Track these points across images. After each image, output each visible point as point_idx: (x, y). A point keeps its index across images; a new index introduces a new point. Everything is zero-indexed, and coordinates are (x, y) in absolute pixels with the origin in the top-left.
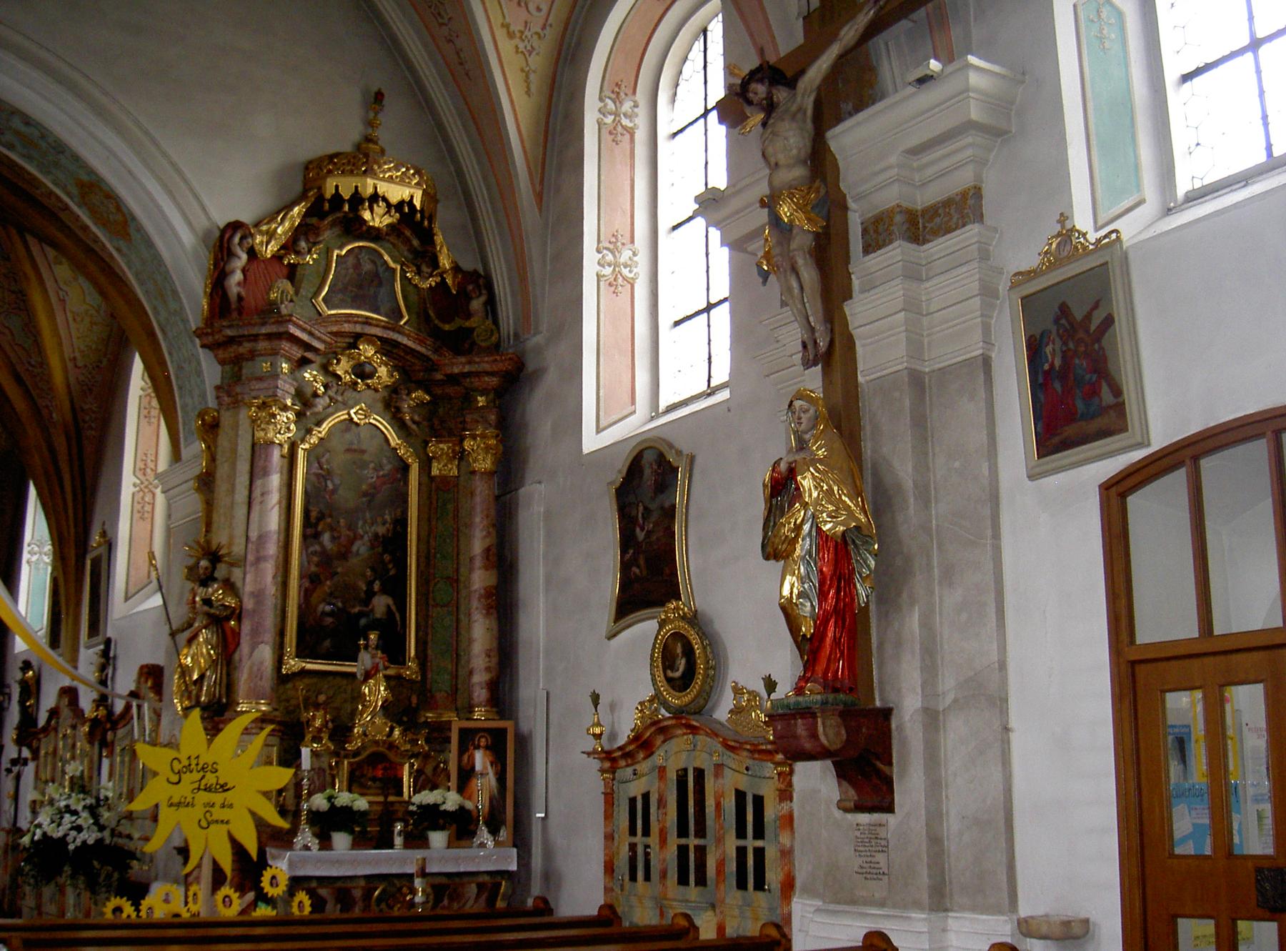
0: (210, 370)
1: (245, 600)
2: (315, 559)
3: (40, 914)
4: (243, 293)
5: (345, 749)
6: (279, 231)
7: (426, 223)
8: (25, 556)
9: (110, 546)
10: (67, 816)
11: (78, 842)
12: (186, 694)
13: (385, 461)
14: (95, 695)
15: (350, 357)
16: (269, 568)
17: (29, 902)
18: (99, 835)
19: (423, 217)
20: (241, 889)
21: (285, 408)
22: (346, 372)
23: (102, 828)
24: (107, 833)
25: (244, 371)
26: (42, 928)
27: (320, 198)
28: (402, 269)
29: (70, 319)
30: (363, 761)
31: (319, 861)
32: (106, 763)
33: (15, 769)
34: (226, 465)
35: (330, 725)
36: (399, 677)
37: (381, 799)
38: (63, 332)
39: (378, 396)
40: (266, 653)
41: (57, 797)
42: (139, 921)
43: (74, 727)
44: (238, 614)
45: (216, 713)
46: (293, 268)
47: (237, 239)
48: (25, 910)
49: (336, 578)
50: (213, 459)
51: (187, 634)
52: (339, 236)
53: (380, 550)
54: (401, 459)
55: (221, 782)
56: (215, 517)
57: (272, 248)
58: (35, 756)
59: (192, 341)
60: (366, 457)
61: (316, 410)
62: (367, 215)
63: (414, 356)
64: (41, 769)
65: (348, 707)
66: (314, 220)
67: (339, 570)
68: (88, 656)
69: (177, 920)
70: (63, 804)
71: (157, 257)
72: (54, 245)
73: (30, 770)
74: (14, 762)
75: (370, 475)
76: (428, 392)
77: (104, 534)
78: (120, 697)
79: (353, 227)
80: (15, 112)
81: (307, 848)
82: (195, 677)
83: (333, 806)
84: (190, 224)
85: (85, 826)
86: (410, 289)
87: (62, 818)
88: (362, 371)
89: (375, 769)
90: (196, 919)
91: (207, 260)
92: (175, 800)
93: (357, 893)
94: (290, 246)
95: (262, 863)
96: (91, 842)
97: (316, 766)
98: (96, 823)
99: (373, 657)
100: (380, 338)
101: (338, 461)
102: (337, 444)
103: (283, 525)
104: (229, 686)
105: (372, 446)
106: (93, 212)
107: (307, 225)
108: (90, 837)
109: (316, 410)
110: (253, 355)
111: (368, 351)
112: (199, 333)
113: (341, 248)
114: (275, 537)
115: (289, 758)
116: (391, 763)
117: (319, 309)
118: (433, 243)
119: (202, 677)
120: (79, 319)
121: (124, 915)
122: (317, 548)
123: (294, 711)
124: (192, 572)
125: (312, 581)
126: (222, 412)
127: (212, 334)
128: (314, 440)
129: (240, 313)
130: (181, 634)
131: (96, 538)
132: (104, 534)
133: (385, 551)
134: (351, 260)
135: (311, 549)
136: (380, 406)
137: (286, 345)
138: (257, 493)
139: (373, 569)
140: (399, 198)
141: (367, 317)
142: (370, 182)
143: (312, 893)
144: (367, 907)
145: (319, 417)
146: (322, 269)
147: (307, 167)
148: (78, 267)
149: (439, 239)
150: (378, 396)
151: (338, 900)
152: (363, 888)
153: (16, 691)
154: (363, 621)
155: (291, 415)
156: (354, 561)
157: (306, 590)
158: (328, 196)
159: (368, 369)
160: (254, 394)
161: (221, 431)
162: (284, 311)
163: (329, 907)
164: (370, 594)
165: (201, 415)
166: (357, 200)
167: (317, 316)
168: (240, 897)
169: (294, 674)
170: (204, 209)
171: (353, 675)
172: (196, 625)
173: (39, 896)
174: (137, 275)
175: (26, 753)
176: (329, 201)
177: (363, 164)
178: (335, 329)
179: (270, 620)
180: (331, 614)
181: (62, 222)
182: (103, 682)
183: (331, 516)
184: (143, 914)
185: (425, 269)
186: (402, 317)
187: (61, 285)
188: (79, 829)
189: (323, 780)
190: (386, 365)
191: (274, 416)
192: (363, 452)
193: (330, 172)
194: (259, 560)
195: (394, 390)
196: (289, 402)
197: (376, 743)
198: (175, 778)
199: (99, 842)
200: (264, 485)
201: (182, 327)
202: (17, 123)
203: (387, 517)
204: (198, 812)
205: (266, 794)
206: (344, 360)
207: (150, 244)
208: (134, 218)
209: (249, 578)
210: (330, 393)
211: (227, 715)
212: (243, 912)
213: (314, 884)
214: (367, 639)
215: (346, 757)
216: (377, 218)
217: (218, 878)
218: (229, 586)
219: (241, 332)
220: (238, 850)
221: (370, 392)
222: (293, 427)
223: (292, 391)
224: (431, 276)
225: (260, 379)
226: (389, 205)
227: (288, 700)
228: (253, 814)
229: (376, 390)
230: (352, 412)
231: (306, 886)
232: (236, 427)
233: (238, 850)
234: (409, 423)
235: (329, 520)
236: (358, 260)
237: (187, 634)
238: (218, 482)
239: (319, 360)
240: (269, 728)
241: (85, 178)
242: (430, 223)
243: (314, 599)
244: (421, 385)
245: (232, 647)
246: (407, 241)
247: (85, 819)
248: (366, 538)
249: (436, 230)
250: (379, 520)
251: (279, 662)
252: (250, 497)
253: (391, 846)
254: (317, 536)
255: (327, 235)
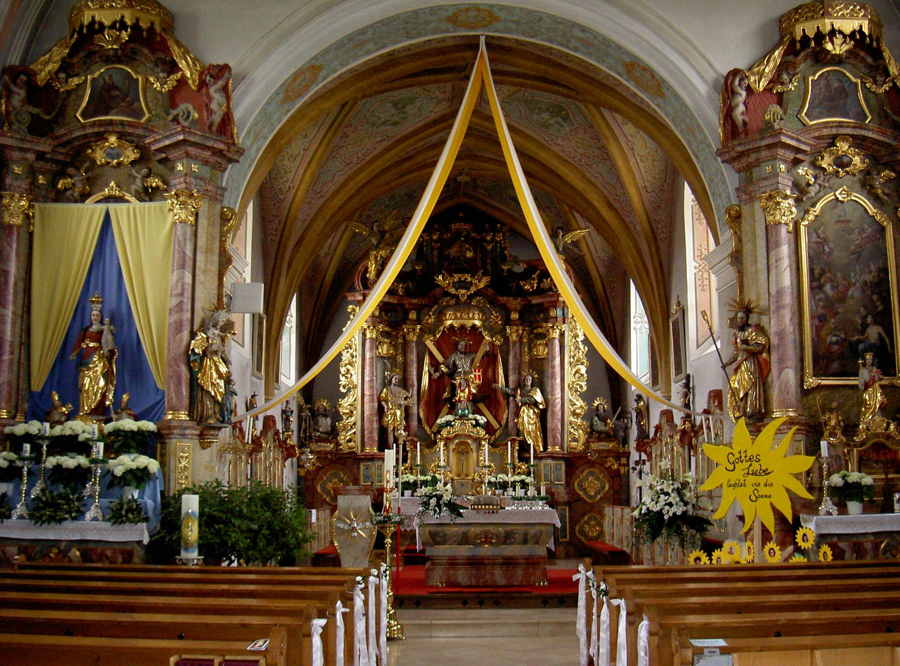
0: (730, 178)
1: (772, 337)
2: (821, 304)
3: (654, 563)
4: (747, 120)
5: (854, 441)
6: (767, 70)
7: (875, 44)
8: (633, 325)
9: (684, 312)
10: (662, 496)
11: (671, 514)
12: (737, 408)
13: (866, 226)
14: (682, 414)
15: (831, 153)
16: (787, 314)
17: (646, 555)
18: (685, 508)
19: (871, 40)
20: (783, 545)
21: (786, 197)
22: (829, 165)
23: (686, 504)
24: (690, 507)
25: (754, 175)
26: (657, 571)
27: (793, 41)
28: (862, 82)
29: (639, 161)
30: (868, 449)
31: (837, 522)
32: (693, 459)
33: (638, 468)
34: (749, 244)
35: (842, 424)
36: (892, 386)
37: (883, 476)
38: (635, 170)
39: (855, 179)
40: (790, 375)
41: (655, 483)
42: (711, 566)
43: (671, 437)
44: (768, 348)
45: (757, 420)
46: (780, 95)
47: (737, 82)
48: (645, 561)
49: (838, 316)
50: (740, 240)
51: (734, 366)
52: (811, 66)
53: (869, 292)
54: (878, 223)
55: (763, 468)
56: (745, 280)
57: (763, 84)
58: (649, 455)
59: (715, 160)
60: (851, 225)
61: (810, 195)
62: (829, 47)
63: (879, 145)
64: (654, 466)
65: (855, 410)
66: (791, 58)
67: (840, 310)
68: (677, 388)
69: (738, 565)
70: (659, 488)
71: (684, 105)
72: (617, 110)
73: (646, 468)
74: (637, 463)
75: (856, 238)
76: (894, 171)
77: (679, 304)
78: (698, 414)
79: (821, 57)
80: (574, 25)
81: (829, 513)
82: (741, 395)
83: (846, 483)
84: (702, 77)
85: (674, 502)
86: (870, 96)
87: (659, 497)
88: (841, 162)
89: (876, 454)
90: (751, 565)
91: (718, 100)
92: (732, 482)
93: (868, 546)
94: (776, 80)
95: (797, 524)
96: (679, 513)
97: (834, 454)
98: (682, 500)
99: (870, 372)
100: (851, 136)
101: (830, 230)
102: (829, 218)
103: (795, 281)
104: (767, 401)
105: (854, 216)
106: (638, 84)
107: (786, 62)
108: (679, 510)
109: (810, 195)
110: (758, 163)
111: (843, 146)
112: (720, 153)
113: (814, 75)
114: (789, 291)
115: (813, 449)
116: (890, 450)
117: (801, 123)
118: (882, 58)
119: (746, 395)
120: (644, 159)
121: (702, 563)
122: (822, 296)
123: (814, 416)
124: (733, 322)
125: (820, 320)
126: (742, 206)
127: (728, 152)
128: (811, 217)
129: (747, 134)
130: (729, 366)
131: (674, 307)
132: (679, 304)
133: (873, 293)
134: (823, 82)
135: (818, 297)
136: (858, 186)
137: (781, 152)
138: (772, 261)
139: (865, 307)
140: (851, 29)
141: (840, 122)
142: (827, 21)
143: (833, 546)
144: (876, 556)
145: (813, 200)
146: (802, 93)
147: (780, 20)
148: (636, 124)
149: (886, 54)
150: (855, 179)
151: (854, 551)
152: (872, 542)
153: (634, 414)
154: (861, 346)
155: (791, 201)
156: (850, 302)
157: (816, 327)
158: (798, 38)
159: (845, 160)
160: (762, 190)
161: (743, 221)
162: (776, 126)
163: (848, 555)
164: (865, 326)
165: (728, 211)
166: (820, 37)
167: (802, 127)
168: (780, 550)
169: (813, 388)
170: (710, 64)
171: (856, 386)
172: (739, 359)
173: (652, 553)
174: (673, 120)
175: (644, 457)
176: (799, 41)
177: (820, 9)
178: (816, 134)
179: (791, 352)
180: (836, 343)
181: (620, 95)
182: (687, 406)
183: (830, 272)
184: (714, 562)
185: (880, 79)
186: (867, 117)
187: (630, 138)
188: (670, 505)
189: (838, 464)
190: (859, 155)
191: (778, 203)
192: (849, 221)
193: (797, 20)
194: (779, 308)
195: (867, 173)
196: (788, 192)
197: (877, 435)
198: (731, 467)
199: (685, 513)
200: (777, 254)
201: (707, 150)
202: (577, 33)
203: (873, 268)
204: (749, 490)
205: (797, 476)
206: (826, 156)
207: (677, 97)
208: (664, 81)
209: (773, 322)
210: (818, 181)
211: (765, 421)
212: (786, 560)
213: (835, 539)
214: (864, 358)
215: (855, 446)
216: (837, 47)
217: (766, 536)
218: (760, 329)
219: (748, 147)
220: (779, 517)
221: (849, 177)
222: (794, 209)
223: (790, 184)
224: (885, 83)
225: (765, 179)
226: (845, 36)
227: (810, 408)
228: (787, 490)
229: (854, 175)
230: (837, 193)
231: (829, 540)
232: (753, 215)
233: (779, 517)
234: (881, 195)
235: (829, 274)
236: (828, 81)
237: (734, 366)
238: (745, 256)
239: (807, 159)
240: (794, 428)
241: (628, 60)
242: (878, 44)
243: (823, 333)
244: (887, 166)
245: (765, 372)
246: (863, 60)
247: (674, 498)
248: (858, 285)
249: (884, 47)
250: (866, 270)
251: (802, 381)
252: (768, 264)
253: (892, 511)
254: (820, 287)
255: (802, 66)
